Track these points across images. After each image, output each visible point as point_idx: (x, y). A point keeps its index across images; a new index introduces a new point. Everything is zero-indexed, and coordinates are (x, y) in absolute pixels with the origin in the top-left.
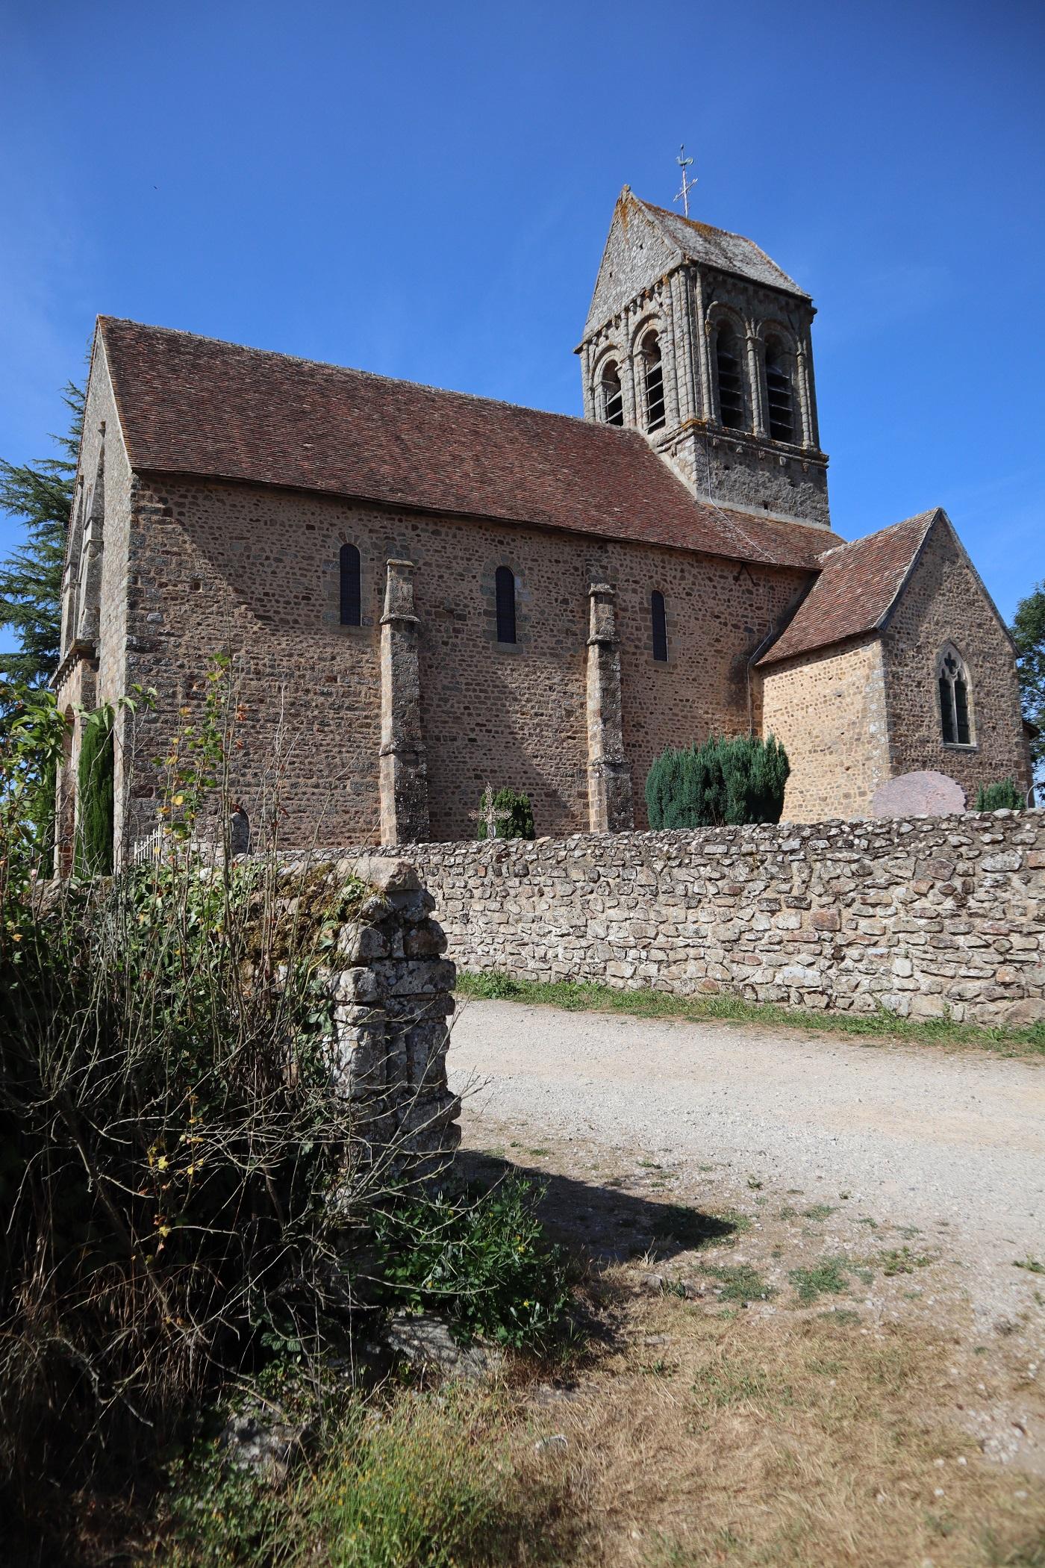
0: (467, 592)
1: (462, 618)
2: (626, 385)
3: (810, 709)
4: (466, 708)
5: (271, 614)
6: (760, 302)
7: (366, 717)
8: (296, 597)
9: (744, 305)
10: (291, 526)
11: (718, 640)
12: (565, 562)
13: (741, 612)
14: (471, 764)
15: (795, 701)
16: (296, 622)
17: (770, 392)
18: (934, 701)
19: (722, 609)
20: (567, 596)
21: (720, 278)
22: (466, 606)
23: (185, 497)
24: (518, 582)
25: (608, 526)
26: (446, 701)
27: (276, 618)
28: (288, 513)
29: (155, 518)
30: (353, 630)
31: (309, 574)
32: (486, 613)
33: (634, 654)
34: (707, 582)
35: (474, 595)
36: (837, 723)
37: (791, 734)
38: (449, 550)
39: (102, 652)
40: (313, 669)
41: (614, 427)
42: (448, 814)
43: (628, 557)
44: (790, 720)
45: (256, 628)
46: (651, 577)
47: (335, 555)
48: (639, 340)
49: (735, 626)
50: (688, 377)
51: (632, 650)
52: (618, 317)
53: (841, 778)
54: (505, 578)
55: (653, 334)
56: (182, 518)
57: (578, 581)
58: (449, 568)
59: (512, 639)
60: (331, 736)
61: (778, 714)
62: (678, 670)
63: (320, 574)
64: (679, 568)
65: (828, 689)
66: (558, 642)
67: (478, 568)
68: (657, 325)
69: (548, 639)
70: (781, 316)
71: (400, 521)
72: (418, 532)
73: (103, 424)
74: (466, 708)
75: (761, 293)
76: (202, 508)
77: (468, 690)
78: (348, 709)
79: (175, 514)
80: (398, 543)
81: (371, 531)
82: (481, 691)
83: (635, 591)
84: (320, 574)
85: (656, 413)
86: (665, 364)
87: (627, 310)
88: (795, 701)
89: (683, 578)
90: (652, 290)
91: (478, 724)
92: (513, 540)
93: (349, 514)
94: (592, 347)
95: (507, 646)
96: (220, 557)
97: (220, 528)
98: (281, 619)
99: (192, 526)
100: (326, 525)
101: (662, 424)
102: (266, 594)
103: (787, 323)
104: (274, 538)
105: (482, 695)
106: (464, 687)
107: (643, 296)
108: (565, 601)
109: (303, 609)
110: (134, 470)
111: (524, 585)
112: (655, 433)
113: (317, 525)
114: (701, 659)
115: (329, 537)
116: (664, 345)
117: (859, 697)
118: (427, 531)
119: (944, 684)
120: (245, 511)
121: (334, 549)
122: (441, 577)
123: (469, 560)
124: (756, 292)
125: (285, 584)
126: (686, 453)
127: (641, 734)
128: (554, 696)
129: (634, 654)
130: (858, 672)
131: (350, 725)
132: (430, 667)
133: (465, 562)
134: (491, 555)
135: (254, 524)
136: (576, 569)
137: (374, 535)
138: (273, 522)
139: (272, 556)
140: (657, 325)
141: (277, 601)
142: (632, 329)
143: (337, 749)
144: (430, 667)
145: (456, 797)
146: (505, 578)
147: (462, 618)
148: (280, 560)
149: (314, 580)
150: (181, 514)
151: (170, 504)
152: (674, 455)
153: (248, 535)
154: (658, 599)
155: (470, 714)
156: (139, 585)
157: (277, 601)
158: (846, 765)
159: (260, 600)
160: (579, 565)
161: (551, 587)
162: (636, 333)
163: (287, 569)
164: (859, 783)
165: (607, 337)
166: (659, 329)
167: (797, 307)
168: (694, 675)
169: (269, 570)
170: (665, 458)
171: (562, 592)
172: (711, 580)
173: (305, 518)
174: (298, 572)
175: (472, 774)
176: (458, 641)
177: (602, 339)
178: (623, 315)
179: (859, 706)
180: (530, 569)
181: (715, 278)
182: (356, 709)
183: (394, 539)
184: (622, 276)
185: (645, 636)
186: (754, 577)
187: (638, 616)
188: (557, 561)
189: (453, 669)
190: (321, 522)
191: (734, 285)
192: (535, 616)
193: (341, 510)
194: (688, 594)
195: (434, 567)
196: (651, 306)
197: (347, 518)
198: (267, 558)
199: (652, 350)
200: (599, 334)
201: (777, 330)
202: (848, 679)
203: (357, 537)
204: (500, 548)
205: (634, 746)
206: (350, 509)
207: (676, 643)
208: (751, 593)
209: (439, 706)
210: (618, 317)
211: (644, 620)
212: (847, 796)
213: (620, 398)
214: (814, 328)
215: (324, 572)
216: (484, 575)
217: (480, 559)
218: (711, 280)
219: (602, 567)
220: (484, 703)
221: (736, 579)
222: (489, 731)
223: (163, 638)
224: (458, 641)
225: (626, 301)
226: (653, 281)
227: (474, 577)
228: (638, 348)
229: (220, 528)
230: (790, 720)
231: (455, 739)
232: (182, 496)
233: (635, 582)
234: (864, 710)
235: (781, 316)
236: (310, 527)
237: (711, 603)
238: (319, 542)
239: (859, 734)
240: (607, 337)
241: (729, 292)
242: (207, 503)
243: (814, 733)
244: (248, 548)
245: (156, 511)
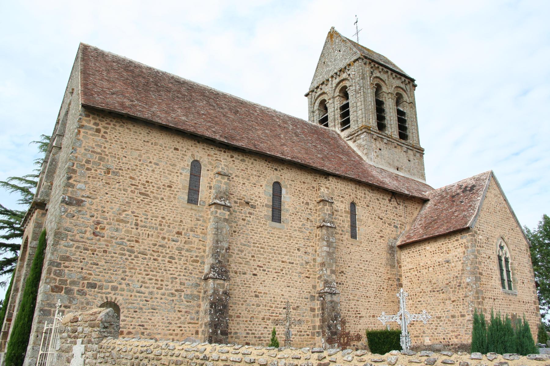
0: (257, 193)
1: (253, 207)
2: (330, 110)
3: (431, 269)
4: (253, 256)
5: (149, 193)
6: (393, 78)
7: (197, 256)
8: (164, 185)
9: (386, 78)
10: (165, 147)
11: (381, 231)
12: (308, 183)
13: (392, 217)
14: (253, 288)
15: (421, 264)
16: (162, 199)
17: (398, 117)
18: (496, 267)
19: (383, 215)
20: (309, 201)
21: (377, 65)
22: (256, 201)
23: (109, 124)
24: (284, 191)
25: (328, 167)
26: (242, 251)
27: (152, 195)
28: (166, 141)
29: (90, 132)
30: (194, 207)
31: (172, 174)
32: (267, 206)
33: (341, 234)
34: (376, 201)
35: (261, 195)
36: (447, 276)
37: (419, 281)
38: (249, 170)
39: (49, 206)
40: (169, 226)
41: (325, 127)
42: (238, 317)
43: (339, 184)
44: (418, 275)
45: (139, 200)
46: (350, 196)
47: (188, 165)
48: (338, 90)
49: (390, 224)
50: (363, 106)
51: (340, 232)
52: (328, 80)
53: (450, 306)
54: (277, 187)
55: (345, 87)
56: (105, 135)
57: (314, 194)
58: (248, 180)
59: (279, 221)
60: (175, 266)
61: (412, 271)
62: (362, 245)
63: (178, 174)
64: (363, 192)
65: (440, 258)
66: (303, 225)
67: (264, 183)
68: (347, 83)
69: (298, 222)
70: (403, 86)
71: (225, 152)
72: (233, 159)
73: (73, 89)
74: (253, 256)
75: (394, 75)
76: (117, 131)
77: (254, 247)
78: (187, 251)
79: (102, 133)
80: (222, 163)
81: (209, 155)
82: (261, 248)
83: (342, 202)
84: (178, 174)
85: (345, 123)
86: (351, 101)
87: (332, 77)
88: (421, 264)
89: (365, 198)
90: (345, 68)
91: (258, 266)
92: (283, 169)
93: (198, 145)
94: (314, 93)
95: (277, 225)
96: (124, 159)
97: (126, 143)
98: (154, 197)
99: (111, 140)
100: (184, 149)
101: (349, 127)
102: (147, 182)
103: (405, 88)
104: (155, 152)
105: (262, 250)
106: (252, 245)
107: (340, 71)
108: (307, 204)
109: (167, 192)
110: (83, 106)
111: (287, 193)
112: (345, 131)
113: (180, 148)
114: (373, 240)
115: (186, 155)
116: (350, 93)
117: (460, 263)
118: (238, 159)
119: (500, 258)
120: (141, 136)
121: (188, 161)
122: (244, 184)
123: (259, 177)
124: (392, 74)
125: (159, 178)
126: (361, 141)
127: (344, 278)
128: (299, 253)
129: (341, 234)
130: (458, 250)
131: (187, 260)
132: (235, 232)
133: (257, 177)
134: (270, 174)
135: (146, 143)
136: (313, 188)
137: (210, 158)
138: (156, 144)
139: (153, 161)
140: (347, 83)
141: (153, 186)
142: (334, 85)
143: (178, 273)
144: (235, 232)
145: (244, 307)
146: (277, 187)
147: (253, 207)
148: (157, 164)
149: (175, 177)
150: (105, 133)
151: (99, 127)
152: (355, 141)
153: (142, 149)
154: (353, 205)
155: (254, 260)
156: (75, 167)
157: (153, 186)
158: (452, 299)
159: (144, 185)
160: (315, 186)
161: (300, 195)
162: (336, 87)
163: (161, 170)
164: (460, 310)
165: (321, 89)
166: (348, 85)
167: (409, 83)
168: (370, 248)
169: (151, 169)
170: (350, 143)
171: (306, 198)
172: (378, 200)
173: (174, 144)
174: (167, 172)
175: (253, 294)
176: (251, 219)
177: (319, 90)
178: (330, 79)
179: (460, 268)
180: (290, 185)
181: (374, 65)
182: (191, 251)
183: (220, 161)
184: (329, 63)
185: (347, 225)
186: (398, 201)
187: (344, 215)
188: (304, 183)
189: (247, 234)
190: (182, 147)
191: (382, 69)
192: (291, 210)
193: (194, 142)
194: (368, 206)
195: (240, 179)
196: (344, 76)
197: (196, 147)
198: (150, 162)
199: (344, 93)
200: (317, 88)
201: (401, 91)
202: (452, 253)
203: (201, 157)
204: (275, 172)
205: (340, 284)
206: (199, 142)
207: (361, 230)
208: (396, 208)
209: (238, 254)
210: (328, 80)
211: (346, 217)
212: (453, 317)
213: (327, 116)
214: (416, 92)
215: (181, 174)
216: (266, 186)
217: (265, 177)
218: (373, 65)
219: (326, 188)
220: (262, 254)
221: (390, 201)
222: (264, 270)
223: (83, 199)
224: (251, 219)
225: (331, 73)
226: (345, 65)
227: (261, 186)
228: (337, 93)
229: (126, 143)
230: (418, 275)
231: (245, 274)
232: (107, 124)
233: (342, 197)
234: (463, 270)
235: (403, 86)
236: (176, 149)
237: (378, 212)
238: (180, 157)
239: (460, 283)
240: (321, 89)
241: (380, 72)
242: (121, 129)
243: (433, 281)
244: (140, 156)
245: (91, 129)
